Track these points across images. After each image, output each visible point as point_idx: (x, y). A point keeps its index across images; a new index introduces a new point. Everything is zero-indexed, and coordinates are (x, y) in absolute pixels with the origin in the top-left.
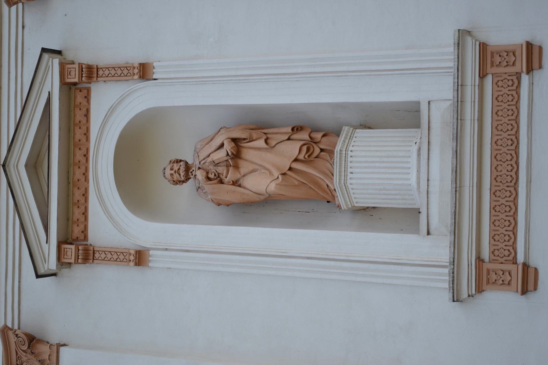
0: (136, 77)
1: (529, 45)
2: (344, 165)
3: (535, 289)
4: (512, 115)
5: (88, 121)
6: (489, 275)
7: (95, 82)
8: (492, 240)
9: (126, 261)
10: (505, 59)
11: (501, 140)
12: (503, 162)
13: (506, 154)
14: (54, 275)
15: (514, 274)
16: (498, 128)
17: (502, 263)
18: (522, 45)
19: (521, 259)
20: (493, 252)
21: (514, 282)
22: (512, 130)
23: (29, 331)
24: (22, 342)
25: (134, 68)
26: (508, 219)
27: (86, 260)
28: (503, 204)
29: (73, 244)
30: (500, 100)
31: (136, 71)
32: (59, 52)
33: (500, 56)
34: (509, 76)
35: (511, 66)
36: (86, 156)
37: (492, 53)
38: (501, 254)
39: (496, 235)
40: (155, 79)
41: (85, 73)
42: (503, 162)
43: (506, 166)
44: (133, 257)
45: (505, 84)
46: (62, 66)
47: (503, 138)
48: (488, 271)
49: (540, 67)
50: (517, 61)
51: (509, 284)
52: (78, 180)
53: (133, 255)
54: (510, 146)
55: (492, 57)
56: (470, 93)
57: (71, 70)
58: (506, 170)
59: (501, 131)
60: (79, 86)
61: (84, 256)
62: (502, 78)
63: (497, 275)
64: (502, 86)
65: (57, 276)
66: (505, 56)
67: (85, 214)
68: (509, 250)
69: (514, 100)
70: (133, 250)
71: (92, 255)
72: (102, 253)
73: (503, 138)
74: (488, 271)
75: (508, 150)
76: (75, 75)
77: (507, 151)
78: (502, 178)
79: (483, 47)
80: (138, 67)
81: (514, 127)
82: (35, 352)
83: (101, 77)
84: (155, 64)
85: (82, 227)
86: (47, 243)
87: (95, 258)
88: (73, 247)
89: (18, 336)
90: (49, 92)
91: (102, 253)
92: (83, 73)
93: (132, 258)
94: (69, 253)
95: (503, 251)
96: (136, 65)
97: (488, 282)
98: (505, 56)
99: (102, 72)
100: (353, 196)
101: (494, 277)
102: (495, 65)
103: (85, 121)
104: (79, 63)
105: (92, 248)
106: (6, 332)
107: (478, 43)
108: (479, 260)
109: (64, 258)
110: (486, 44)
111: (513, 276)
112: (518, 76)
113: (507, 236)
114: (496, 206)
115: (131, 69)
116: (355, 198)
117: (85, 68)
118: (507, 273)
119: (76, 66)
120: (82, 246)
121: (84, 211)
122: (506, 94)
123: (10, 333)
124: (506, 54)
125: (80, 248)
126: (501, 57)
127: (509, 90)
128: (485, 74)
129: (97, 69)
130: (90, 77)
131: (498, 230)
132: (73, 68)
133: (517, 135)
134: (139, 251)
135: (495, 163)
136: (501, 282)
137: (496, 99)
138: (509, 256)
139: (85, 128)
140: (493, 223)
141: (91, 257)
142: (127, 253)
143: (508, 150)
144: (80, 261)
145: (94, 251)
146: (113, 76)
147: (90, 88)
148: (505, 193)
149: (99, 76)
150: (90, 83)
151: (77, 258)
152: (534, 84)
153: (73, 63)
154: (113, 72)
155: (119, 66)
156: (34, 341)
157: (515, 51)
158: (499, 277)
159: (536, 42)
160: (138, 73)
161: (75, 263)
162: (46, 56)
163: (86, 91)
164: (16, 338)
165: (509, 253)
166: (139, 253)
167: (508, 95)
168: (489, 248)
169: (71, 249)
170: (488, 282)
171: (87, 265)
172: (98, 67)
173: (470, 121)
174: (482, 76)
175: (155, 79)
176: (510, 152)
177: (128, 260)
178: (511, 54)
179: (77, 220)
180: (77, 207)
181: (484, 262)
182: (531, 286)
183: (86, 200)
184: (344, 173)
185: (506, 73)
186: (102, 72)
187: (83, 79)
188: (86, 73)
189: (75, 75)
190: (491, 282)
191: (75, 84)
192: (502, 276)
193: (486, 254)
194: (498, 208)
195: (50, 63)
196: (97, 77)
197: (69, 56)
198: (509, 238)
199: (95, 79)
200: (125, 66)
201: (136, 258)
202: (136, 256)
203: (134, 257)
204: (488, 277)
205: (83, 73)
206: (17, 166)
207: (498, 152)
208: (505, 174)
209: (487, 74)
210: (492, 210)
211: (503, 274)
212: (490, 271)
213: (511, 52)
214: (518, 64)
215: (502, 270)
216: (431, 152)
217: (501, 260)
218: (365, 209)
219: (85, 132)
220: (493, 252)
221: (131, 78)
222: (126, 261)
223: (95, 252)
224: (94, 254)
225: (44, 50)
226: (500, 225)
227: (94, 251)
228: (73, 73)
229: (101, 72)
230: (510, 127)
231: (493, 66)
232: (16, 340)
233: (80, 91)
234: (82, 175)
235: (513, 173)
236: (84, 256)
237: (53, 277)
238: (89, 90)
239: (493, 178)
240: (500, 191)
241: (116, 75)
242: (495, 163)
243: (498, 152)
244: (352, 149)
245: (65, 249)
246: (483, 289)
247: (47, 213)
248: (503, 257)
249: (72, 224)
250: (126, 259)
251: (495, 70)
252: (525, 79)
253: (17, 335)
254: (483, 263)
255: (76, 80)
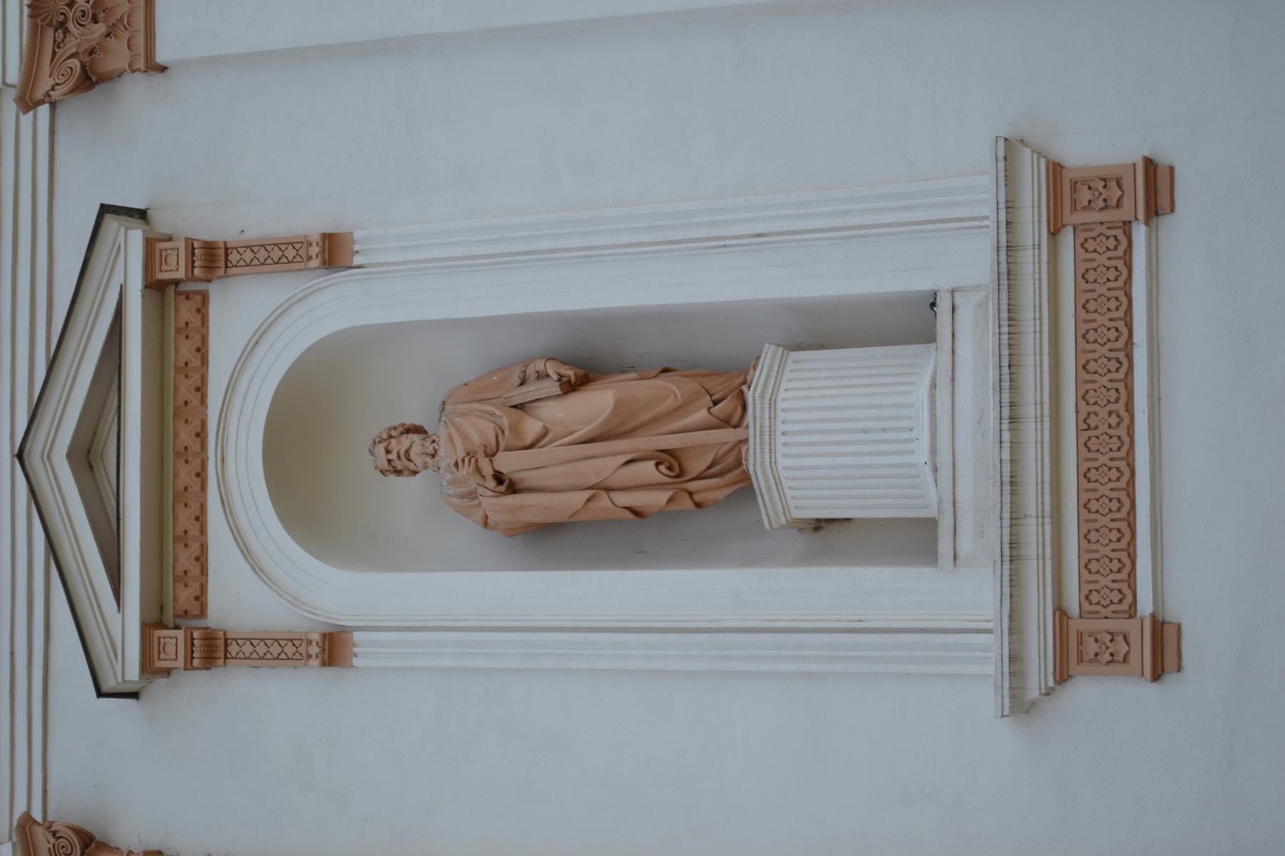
0: (315, 263)
1: (1150, 164)
2: (768, 433)
3: (1172, 210)
4: (1117, 309)
5: (204, 361)
6: (1081, 644)
7: (221, 277)
8: (1084, 542)
9: (300, 657)
10: (1101, 194)
11: (1095, 270)
12: (1103, 606)
13: (1106, 390)
14: (134, 695)
15: (1134, 638)
16: (1087, 336)
17: (1106, 618)
18: (1134, 165)
19: (1145, 606)
20: (1087, 597)
21: (1135, 656)
22: (1117, 370)
23: (76, 821)
24: (67, 847)
25: (310, 244)
26: (1116, 588)
27: (209, 660)
28: (1102, 294)
29: (181, 629)
30: (1092, 401)
31: (315, 250)
32: (142, 215)
33: (1090, 188)
34: (1108, 228)
35: (1119, 662)
36: (201, 435)
37: (1074, 184)
38: (1105, 599)
39: (1093, 561)
40: (359, 267)
41: (199, 258)
42: (1103, 606)
43: (1106, 416)
44: (317, 648)
45: (1104, 536)
46: (149, 244)
47: (1100, 358)
48: (1080, 635)
49: (1179, 668)
50: (1132, 654)
51: (1125, 660)
52: (186, 403)
53: (317, 643)
54: (1113, 250)
55: (1080, 642)
56: (1031, 264)
57: (170, 254)
58: (1106, 425)
59: (1094, 312)
60: (183, 287)
61: (205, 651)
62: (1094, 234)
63: (1099, 644)
64: (1095, 251)
65: (141, 700)
66: (1101, 188)
67: (201, 559)
68: (1120, 591)
69: (1120, 279)
70: (315, 632)
71: (222, 649)
72: (244, 644)
73: (1100, 358)
74: (1080, 635)
75: (1110, 381)
76: (178, 263)
77: (1109, 322)
78: (1099, 442)
79: (1055, 170)
80: (319, 641)
81: (1125, 596)
82: (98, 53)
83: (236, 266)
84: (358, 234)
85: (194, 588)
86: (119, 611)
87: (229, 656)
88: (180, 634)
89: (58, 835)
90: (121, 286)
91: (244, 644)
92: (195, 258)
93: (314, 650)
94: (170, 649)
95: (1104, 271)
96: (315, 237)
97: (1081, 660)
98: (1101, 188)
99: (238, 257)
100: (789, 493)
101: (1092, 648)
102: (1079, 207)
103: (197, 448)
104: (187, 239)
105: (221, 635)
106: (29, 828)
107: (1043, 161)
108: (1061, 612)
109: (161, 271)
110: (1060, 165)
111: (1132, 644)
112: (1127, 226)
113: (1114, 471)
114: (1091, 591)
115: (303, 644)
116: (793, 498)
117: (197, 639)
118: (1114, 183)
119: (182, 246)
120: (201, 631)
121: (198, 553)
122: (1104, 266)
123: (40, 832)
124: (1110, 637)
125: (196, 634)
126: (1092, 191)
127: (1109, 259)
128: (1060, 225)
129: (226, 249)
130: (210, 265)
131: (1097, 551)
132: (173, 249)
133: (1131, 519)
134: (331, 634)
135: (1084, 409)
136: (1108, 658)
137: (1084, 307)
138: (1120, 601)
139: (198, 461)
140: (1085, 537)
141: (221, 654)
142: (302, 640)
143: (1110, 381)
144: (196, 662)
145: (226, 640)
146: (262, 264)
147: (207, 292)
148: (1109, 363)
149: (231, 265)
150: (209, 281)
151: (190, 656)
152: (1162, 402)
153: (170, 239)
154: (262, 254)
155: (275, 243)
156: (93, 845)
157: (1122, 178)
158: (1103, 647)
159: (1163, 159)
160: (320, 256)
161: (186, 669)
162: (111, 222)
163: (199, 297)
164: (52, 840)
165: (1120, 596)
166: (330, 639)
167: (1108, 269)
168: (1079, 557)
169: (174, 640)
170: (1081, 660)
171: (214, 670)
172: (229, 246)
173: (1030, 225)
174: (1054, 233)
175: (359, 267)
176: (1114, 263)
177: (304, 655)
178: (1121, 638)
179: (183, 534)
180: (182, 545)
181: (1070, 618)
182: (1163, 201)
183: (203, 530)
184: (770, 412)
185: (1101, 223)
186: (238, 257)
187: (197, 272)
188: (201, 258)
189: (178, 263)
190: (1085, 658)
191: (177, 283)
192: (1108, 644)
193: (1073, 601)
194: (1094, 505)
195: (121, 239)
196: (227, 267)
197: (163, 222)
198: (1119, 474)
199: (221, 271)
200: (288, 242)
201: (323, 252)
202: (324, 246)
203: (320, 647)
204: (1074, 196)
205: (195, 258)
206: (49, 457)
207: (1093, 586)
208: (1107, 587)
209: (1071, 676)
210: (1082, 508)
211: (1105, 187)
212: (1083, 635)
213: (1111, 179)
214: (1127, 204)
215: (1110, 633)
216: (952, 525)
217: (1104, 612)
218: (819, 525)
219: (199, 384)
220: (1087, 597)
221: (302, 266)
222: (300, 657)
223: (229, 641)
224: (227, 255)
225: (105, 210)
226: (1101, 539)
227: (226, 640)
228: (172, 260)
229: (234, 257)
230: (1113, 335)
231: (1075, 210)
232: (51, 846)
233: (187, 298)
234: (193, 562)
235: (1122, 432)
236: (205, 651)
237: (130, 702)
238: (205, 296)
239: (1080, 395)
240: (1097, 469)
241: (268, 656)
242: (1084, 409)
243: (1089, 386)
244: (785, 430)
245: (162, 640)
246: (1064, 223)
247: (117, 576)
248: (1108, 606)
249: (173, 503)
250: (301, 654)
251: (1080, 217)
252: (1140, 233)
253: (54, 833)
254: (1070, 620)
255: (181, 274)
